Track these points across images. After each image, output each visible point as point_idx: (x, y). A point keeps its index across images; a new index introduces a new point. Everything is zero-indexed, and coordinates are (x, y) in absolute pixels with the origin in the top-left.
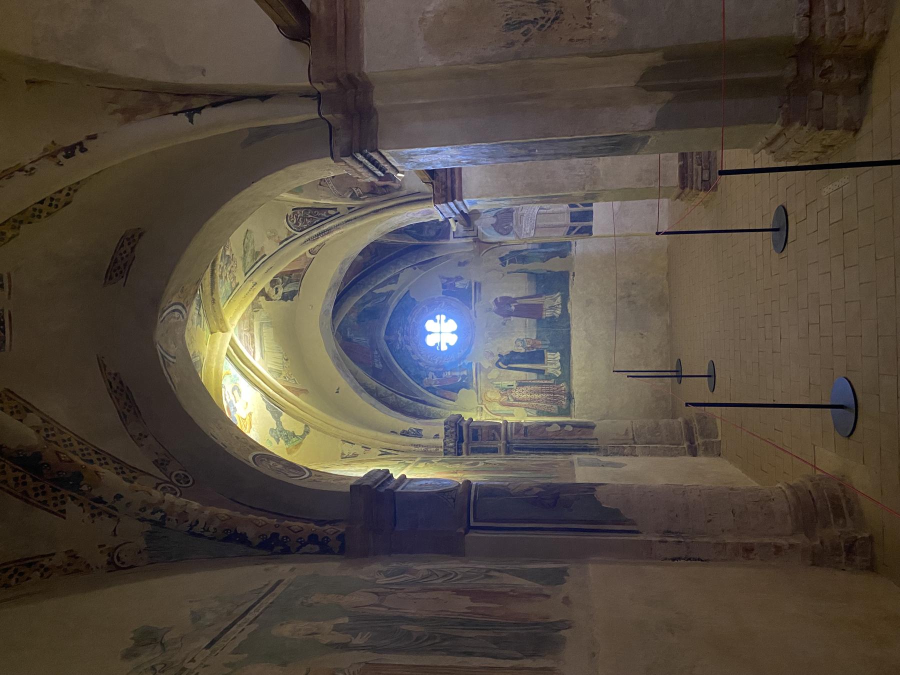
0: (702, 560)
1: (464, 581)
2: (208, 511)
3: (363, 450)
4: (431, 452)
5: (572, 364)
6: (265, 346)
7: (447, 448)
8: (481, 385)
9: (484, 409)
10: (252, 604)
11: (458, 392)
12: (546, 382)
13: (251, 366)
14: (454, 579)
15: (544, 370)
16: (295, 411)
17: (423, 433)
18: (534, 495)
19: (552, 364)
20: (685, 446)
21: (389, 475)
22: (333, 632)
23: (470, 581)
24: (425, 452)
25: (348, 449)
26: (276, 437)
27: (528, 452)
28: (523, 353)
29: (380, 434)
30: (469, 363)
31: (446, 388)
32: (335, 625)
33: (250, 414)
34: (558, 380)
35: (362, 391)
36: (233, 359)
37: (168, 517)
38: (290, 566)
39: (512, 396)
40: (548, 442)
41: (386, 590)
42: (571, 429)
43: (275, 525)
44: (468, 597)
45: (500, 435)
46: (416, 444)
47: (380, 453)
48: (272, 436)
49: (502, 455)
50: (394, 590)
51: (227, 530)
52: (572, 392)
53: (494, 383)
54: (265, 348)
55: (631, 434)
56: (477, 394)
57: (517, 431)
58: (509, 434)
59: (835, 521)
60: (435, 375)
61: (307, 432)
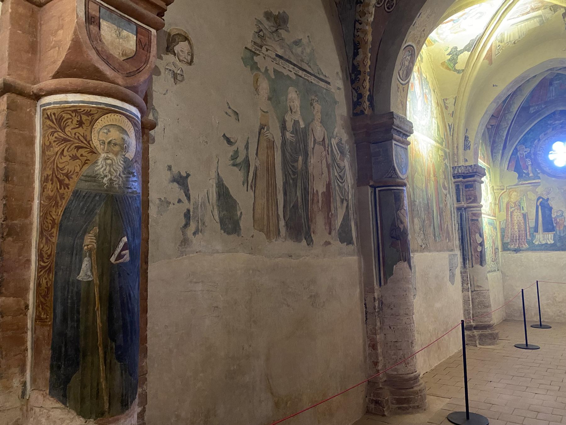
0: (366, 320)
1: (337, 188)
2: (368, 28)
3: (451, 112)
4: (454, 158)
5: (545, 252)
6: (522, 25)
7: (457, 169)
8: (522, 188)
9: (503, 191)
10: (310, 71)
11: (515, 171)
12: (528, 234)
13: (501, 19)
14: (338, 182)
15: (537, 232)
16: (473, 60)
17: (468, 151)
18: (398, 225)
19: (544, 237)
20: (472, 323)
21: (408, 134)
22: (293, 120)
23: (337, 191)
24: (454, 154)
25: (451, 101)
26: (451, 52)
27: (459, 222)
28: (551, 216)
29: (463, 121)
30: (540, 177)
31: (517, 162)
32: (298, 122)
33: (464, 30)
34: (530, 243)
35: (498, 102)
36: (503, 6)
37: (361, 5)
38: (342, 86)
39: (515, 210)
40: (468, 235)
41: (327, 146)
42: (189, 216)
43: (365, 71)
44: (325, 191)
45: (470, 203)
46: (459, 147)
47: (450, 124)
48: (452, 49)
49: (455, 206)
50: (327, 149)
51: (359, 43)
52: (521, 252)
53: (524, 197)
54: (520, 25)
55: (478, 289)
56: (514, 185)
57: (474, 215)
58: (472, 209)
59: (395, 398)
60: (528, 153)
61: (459, 72)
